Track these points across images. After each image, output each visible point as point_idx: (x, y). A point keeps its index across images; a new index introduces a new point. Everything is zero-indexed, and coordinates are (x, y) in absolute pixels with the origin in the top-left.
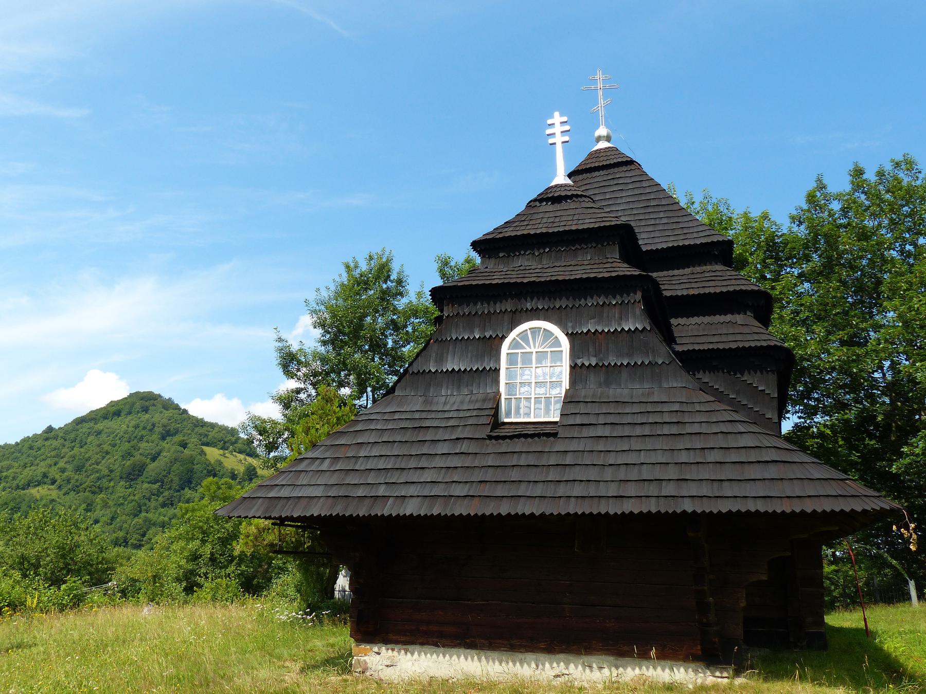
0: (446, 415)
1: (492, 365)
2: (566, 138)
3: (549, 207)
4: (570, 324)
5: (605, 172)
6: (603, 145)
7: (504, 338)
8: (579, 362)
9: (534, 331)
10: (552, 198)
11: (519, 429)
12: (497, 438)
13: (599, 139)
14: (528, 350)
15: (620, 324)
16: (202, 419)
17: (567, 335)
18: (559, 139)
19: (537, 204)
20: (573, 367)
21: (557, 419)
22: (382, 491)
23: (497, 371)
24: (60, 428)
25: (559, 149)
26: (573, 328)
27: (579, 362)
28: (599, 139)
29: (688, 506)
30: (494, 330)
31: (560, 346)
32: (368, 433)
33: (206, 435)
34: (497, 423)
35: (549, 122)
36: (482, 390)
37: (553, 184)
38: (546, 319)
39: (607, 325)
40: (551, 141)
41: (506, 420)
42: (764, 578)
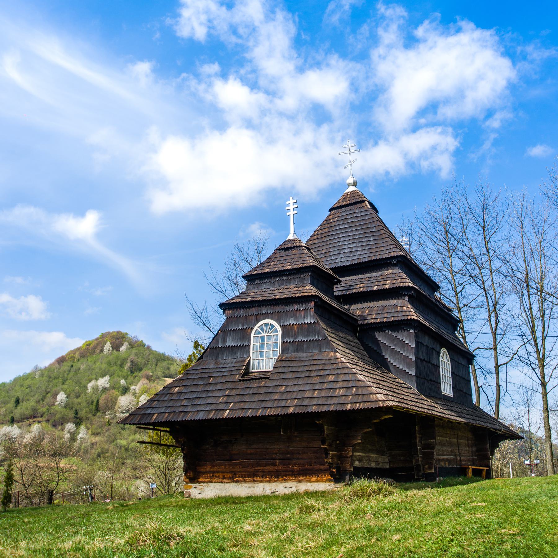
0: (224, 370)
1: (247, 343)
2: (295, 212)
3: (283, 253)
4: (282, 321)
5: (347, 208)
6: (352, 189)
7: (252, 329)
8: (285, 340)
9: (266, 324)
10: (287, 248)
11: (261, 375)
12: (243, 380)
13: (349, 185)
14: (263, 335)
15: (304, 320)
16: (163, 354)
17: (280, 326)
18: (292, 213)
19: (278, 252)
20: (283, 343)
21: (271, 369)
22: (189, 409)
23: (249, 346)
24: (46, 368)
25: (292, 217)
26: (283, 323)
27: (285, 340)
28: (349, 185)
29: (314, 409)
30: (248, 325)
31: (277, 332)
32: (188, 380)
33: (169, 368)
34: (247, 372)
35: (288, 203)
36: (239, 355)
37: (288, 239)
38: (272, 319)
39: (298, 321)
40: (288, 214)
41: (253, 371)
42: (359, 441)
